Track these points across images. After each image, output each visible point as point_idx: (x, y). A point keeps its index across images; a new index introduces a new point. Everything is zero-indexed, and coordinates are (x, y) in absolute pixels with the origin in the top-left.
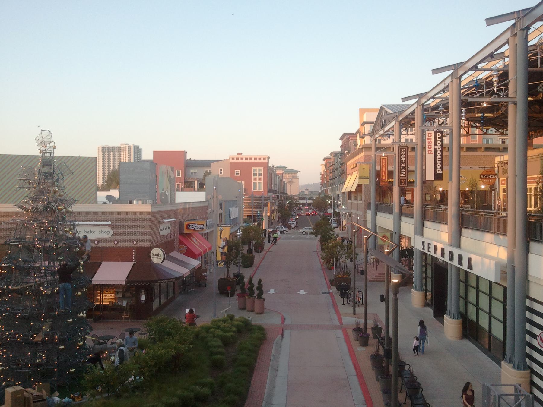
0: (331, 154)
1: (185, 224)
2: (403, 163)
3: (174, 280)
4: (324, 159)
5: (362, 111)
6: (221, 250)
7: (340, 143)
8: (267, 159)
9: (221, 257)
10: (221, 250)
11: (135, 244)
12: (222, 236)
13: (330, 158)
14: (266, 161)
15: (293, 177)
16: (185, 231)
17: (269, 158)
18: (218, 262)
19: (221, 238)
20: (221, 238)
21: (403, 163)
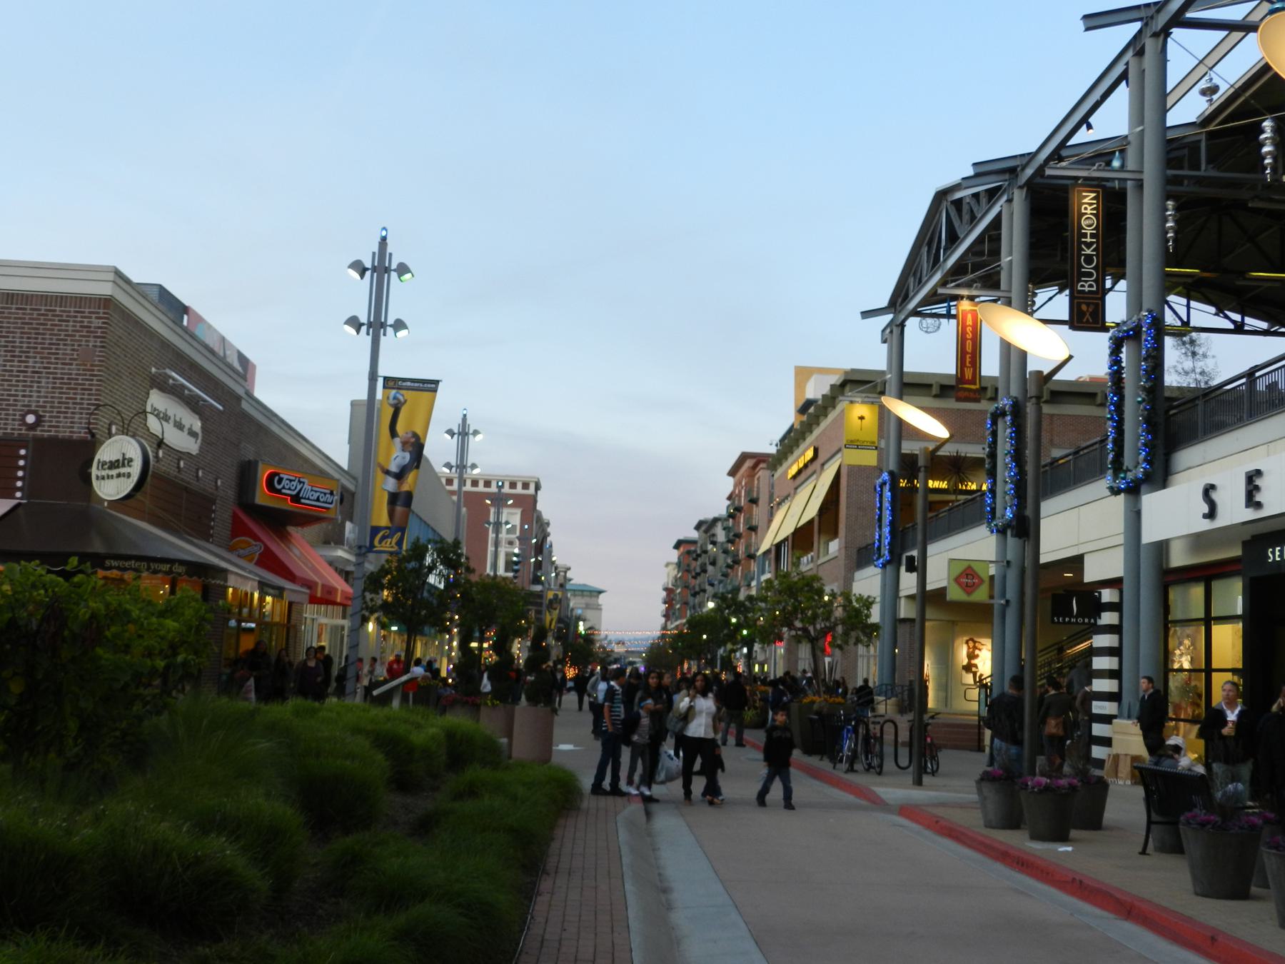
0: (698, 527)
1: (263, 474)
2: (1089, 245)
3: (179, 569)
4: (678, 545)
5: (803, 374)
6: (391, 484)
7: (728, 484)
8: (532, 487)
9: (391, 514)
10: (391, 484)
11: (32, 427)
12: (400, 428)
13: (694, 542)
14: (531, 490)
15: (588, 607)
16: (262, 497)
17: (538, 487)
18: (375, 530)
19: (393, 433)
20: (393, 433)
21: (1089, 245)
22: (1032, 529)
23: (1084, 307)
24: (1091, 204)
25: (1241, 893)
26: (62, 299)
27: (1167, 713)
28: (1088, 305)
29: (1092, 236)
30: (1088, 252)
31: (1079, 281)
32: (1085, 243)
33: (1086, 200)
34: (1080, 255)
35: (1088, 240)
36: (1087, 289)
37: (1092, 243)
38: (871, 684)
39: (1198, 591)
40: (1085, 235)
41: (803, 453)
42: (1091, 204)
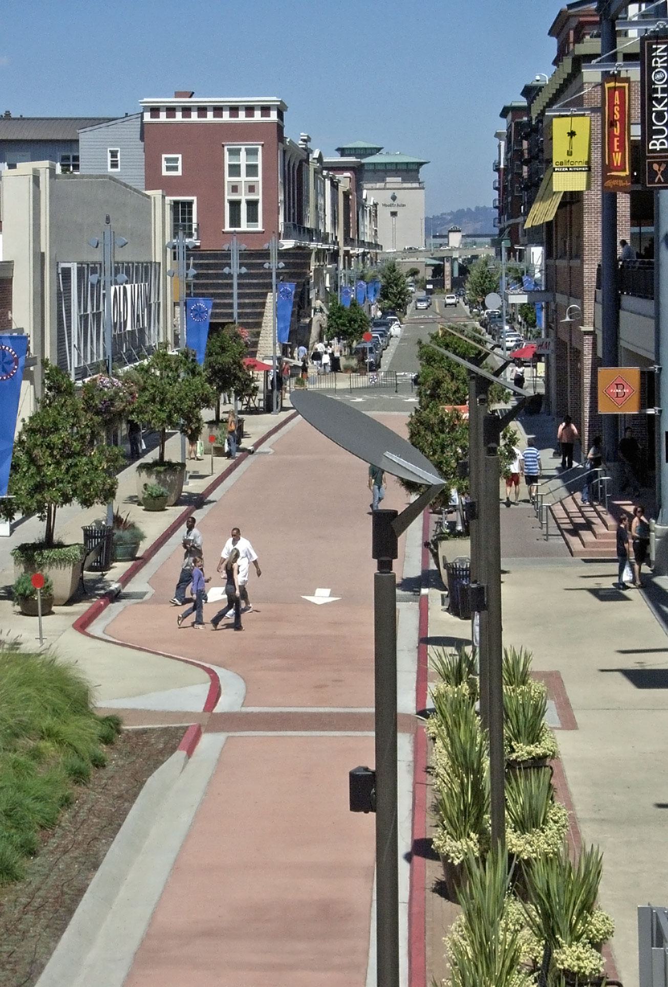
21: (659, 101)
22: (492, 604)
23: (656, 167)
24: (661, 57)
25: (77, 141)
26: (50, 224)
27: (480, 679)
28: (660, 164)
29: (663, 90)
30: (659, 108)
31: (651, 139)
32: (656, 99)
33: (658, 53)
34: (651, 113)
35: (659, 95)
36: (658, 148)
37: (663, 99)
38: (231, 539)
39: (226, 703)
40: (656, 91)
41: (465, 736)
42: (661, 57)
